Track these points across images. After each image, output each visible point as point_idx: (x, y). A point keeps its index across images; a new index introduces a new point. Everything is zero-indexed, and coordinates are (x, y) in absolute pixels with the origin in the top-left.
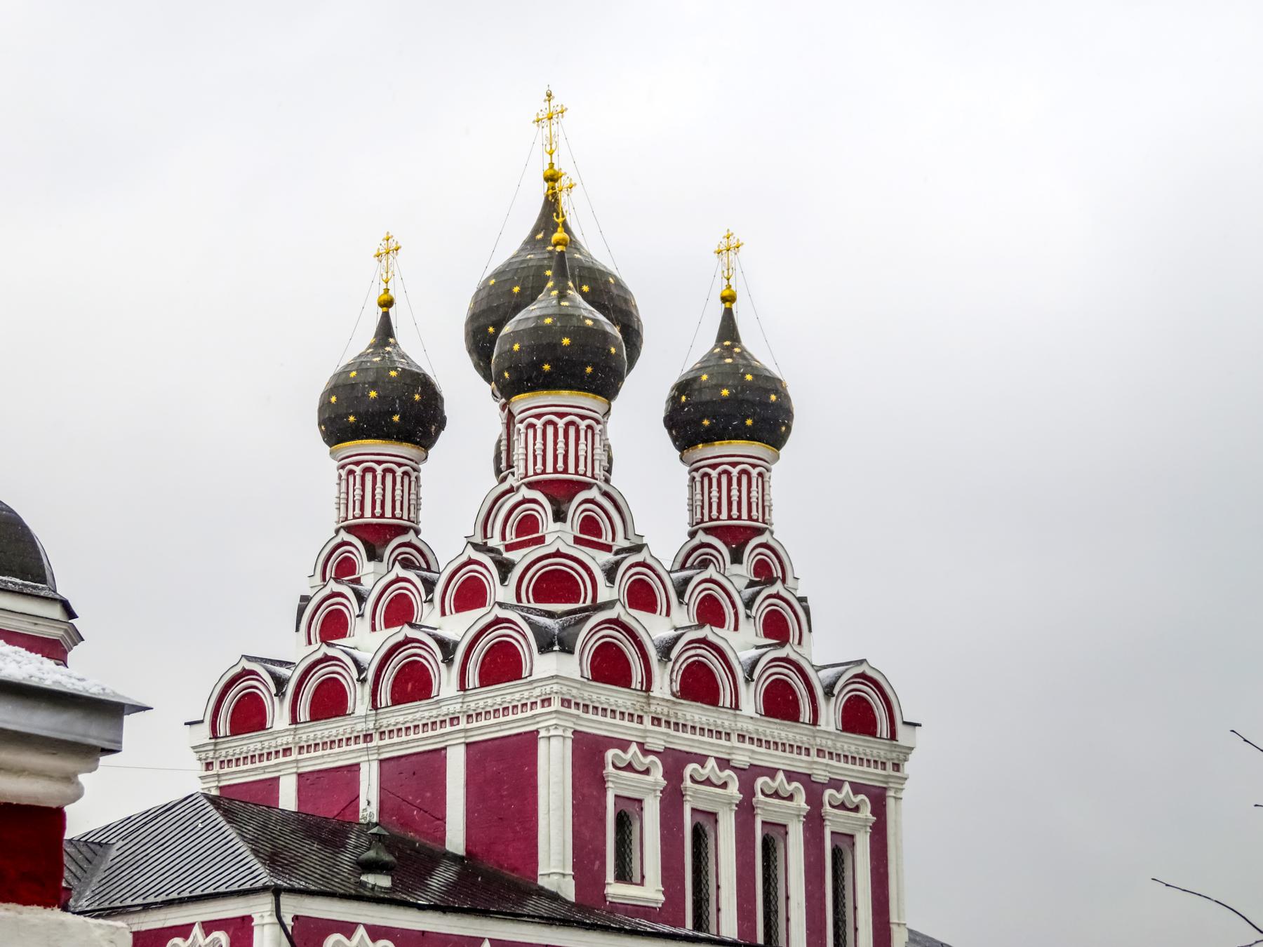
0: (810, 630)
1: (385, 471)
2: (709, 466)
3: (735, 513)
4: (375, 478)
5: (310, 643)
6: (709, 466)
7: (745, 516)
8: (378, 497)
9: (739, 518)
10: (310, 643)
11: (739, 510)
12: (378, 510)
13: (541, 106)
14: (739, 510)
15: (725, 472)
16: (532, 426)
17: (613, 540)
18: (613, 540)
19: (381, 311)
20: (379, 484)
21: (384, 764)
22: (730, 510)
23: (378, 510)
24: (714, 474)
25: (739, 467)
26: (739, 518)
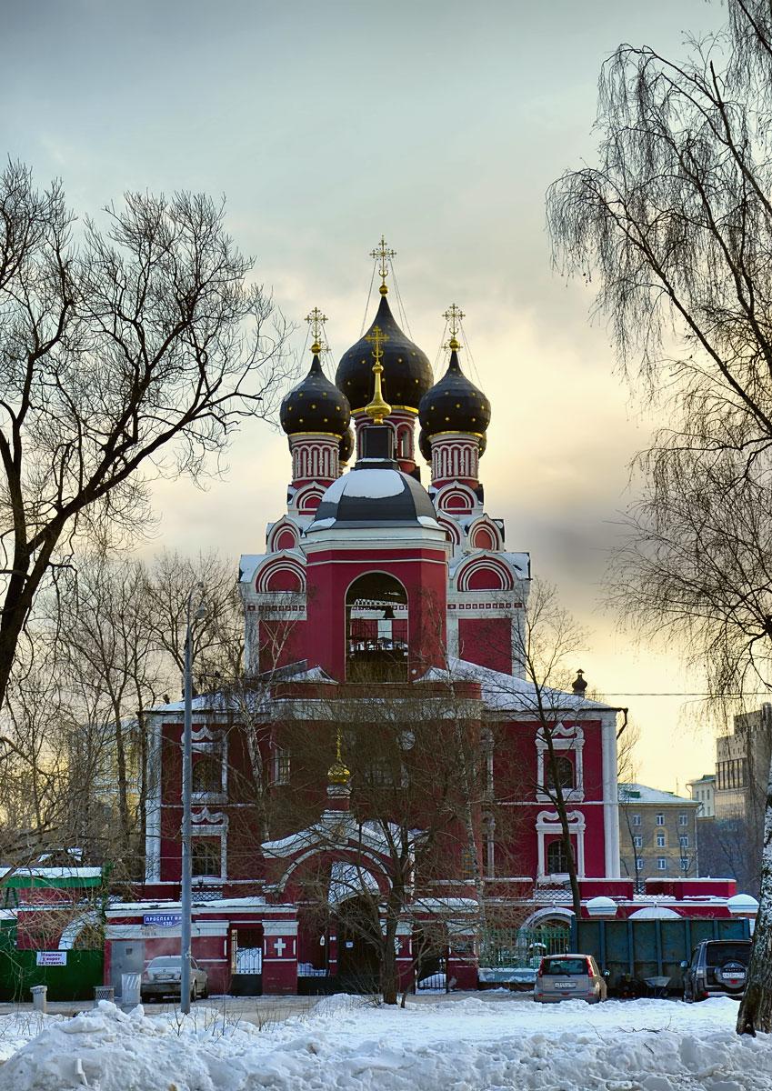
0: (504, 541)
1: (324, 449)
2: (318, 444)
3: (321, 473)
4: (318, 453)
5: (273, 551)
6: (318, 444)
7: (326, 475)
8: (321, 465)
9: (323, 476)
10: (273, 551)
11: (323, 471)
12: (450, 473)
13: (376, 246)
14: (323, 471)
15: (456, 448)
16: (305, 449)
17: (472, 506)
18: (472, 506)
19: (313, 355)
20: (321, 456)
21: (395, 623)
22: (460, 470)
23: (450, 473)
24: (450, 448)
25: (465, 446)
26: (323, 476)
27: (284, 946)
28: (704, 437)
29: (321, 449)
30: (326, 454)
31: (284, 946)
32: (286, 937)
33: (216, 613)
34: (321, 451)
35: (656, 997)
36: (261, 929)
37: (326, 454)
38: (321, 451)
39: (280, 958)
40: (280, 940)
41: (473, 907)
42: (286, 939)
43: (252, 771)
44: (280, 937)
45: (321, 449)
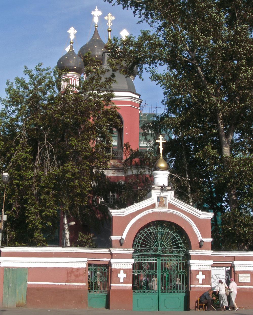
4: (72, 80)
27: (204, 277)
28: (59, 210)
29: (73, 79)
30: (75, 81)
31: (204, 277)
32: (205, 271)
33: (40, 167)
34: (73, 80)
35: (106, 302)
36: (110, 264)
37: (75, 81)
38: (73, 80)
39: (200, 284)
40: (201, 273)
41: (70, 273)
42: (125, 271)
43: (34, 234)
44: (122, 269)
45: (73, 79)
